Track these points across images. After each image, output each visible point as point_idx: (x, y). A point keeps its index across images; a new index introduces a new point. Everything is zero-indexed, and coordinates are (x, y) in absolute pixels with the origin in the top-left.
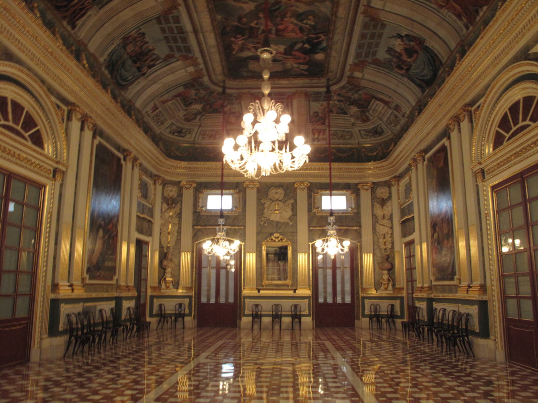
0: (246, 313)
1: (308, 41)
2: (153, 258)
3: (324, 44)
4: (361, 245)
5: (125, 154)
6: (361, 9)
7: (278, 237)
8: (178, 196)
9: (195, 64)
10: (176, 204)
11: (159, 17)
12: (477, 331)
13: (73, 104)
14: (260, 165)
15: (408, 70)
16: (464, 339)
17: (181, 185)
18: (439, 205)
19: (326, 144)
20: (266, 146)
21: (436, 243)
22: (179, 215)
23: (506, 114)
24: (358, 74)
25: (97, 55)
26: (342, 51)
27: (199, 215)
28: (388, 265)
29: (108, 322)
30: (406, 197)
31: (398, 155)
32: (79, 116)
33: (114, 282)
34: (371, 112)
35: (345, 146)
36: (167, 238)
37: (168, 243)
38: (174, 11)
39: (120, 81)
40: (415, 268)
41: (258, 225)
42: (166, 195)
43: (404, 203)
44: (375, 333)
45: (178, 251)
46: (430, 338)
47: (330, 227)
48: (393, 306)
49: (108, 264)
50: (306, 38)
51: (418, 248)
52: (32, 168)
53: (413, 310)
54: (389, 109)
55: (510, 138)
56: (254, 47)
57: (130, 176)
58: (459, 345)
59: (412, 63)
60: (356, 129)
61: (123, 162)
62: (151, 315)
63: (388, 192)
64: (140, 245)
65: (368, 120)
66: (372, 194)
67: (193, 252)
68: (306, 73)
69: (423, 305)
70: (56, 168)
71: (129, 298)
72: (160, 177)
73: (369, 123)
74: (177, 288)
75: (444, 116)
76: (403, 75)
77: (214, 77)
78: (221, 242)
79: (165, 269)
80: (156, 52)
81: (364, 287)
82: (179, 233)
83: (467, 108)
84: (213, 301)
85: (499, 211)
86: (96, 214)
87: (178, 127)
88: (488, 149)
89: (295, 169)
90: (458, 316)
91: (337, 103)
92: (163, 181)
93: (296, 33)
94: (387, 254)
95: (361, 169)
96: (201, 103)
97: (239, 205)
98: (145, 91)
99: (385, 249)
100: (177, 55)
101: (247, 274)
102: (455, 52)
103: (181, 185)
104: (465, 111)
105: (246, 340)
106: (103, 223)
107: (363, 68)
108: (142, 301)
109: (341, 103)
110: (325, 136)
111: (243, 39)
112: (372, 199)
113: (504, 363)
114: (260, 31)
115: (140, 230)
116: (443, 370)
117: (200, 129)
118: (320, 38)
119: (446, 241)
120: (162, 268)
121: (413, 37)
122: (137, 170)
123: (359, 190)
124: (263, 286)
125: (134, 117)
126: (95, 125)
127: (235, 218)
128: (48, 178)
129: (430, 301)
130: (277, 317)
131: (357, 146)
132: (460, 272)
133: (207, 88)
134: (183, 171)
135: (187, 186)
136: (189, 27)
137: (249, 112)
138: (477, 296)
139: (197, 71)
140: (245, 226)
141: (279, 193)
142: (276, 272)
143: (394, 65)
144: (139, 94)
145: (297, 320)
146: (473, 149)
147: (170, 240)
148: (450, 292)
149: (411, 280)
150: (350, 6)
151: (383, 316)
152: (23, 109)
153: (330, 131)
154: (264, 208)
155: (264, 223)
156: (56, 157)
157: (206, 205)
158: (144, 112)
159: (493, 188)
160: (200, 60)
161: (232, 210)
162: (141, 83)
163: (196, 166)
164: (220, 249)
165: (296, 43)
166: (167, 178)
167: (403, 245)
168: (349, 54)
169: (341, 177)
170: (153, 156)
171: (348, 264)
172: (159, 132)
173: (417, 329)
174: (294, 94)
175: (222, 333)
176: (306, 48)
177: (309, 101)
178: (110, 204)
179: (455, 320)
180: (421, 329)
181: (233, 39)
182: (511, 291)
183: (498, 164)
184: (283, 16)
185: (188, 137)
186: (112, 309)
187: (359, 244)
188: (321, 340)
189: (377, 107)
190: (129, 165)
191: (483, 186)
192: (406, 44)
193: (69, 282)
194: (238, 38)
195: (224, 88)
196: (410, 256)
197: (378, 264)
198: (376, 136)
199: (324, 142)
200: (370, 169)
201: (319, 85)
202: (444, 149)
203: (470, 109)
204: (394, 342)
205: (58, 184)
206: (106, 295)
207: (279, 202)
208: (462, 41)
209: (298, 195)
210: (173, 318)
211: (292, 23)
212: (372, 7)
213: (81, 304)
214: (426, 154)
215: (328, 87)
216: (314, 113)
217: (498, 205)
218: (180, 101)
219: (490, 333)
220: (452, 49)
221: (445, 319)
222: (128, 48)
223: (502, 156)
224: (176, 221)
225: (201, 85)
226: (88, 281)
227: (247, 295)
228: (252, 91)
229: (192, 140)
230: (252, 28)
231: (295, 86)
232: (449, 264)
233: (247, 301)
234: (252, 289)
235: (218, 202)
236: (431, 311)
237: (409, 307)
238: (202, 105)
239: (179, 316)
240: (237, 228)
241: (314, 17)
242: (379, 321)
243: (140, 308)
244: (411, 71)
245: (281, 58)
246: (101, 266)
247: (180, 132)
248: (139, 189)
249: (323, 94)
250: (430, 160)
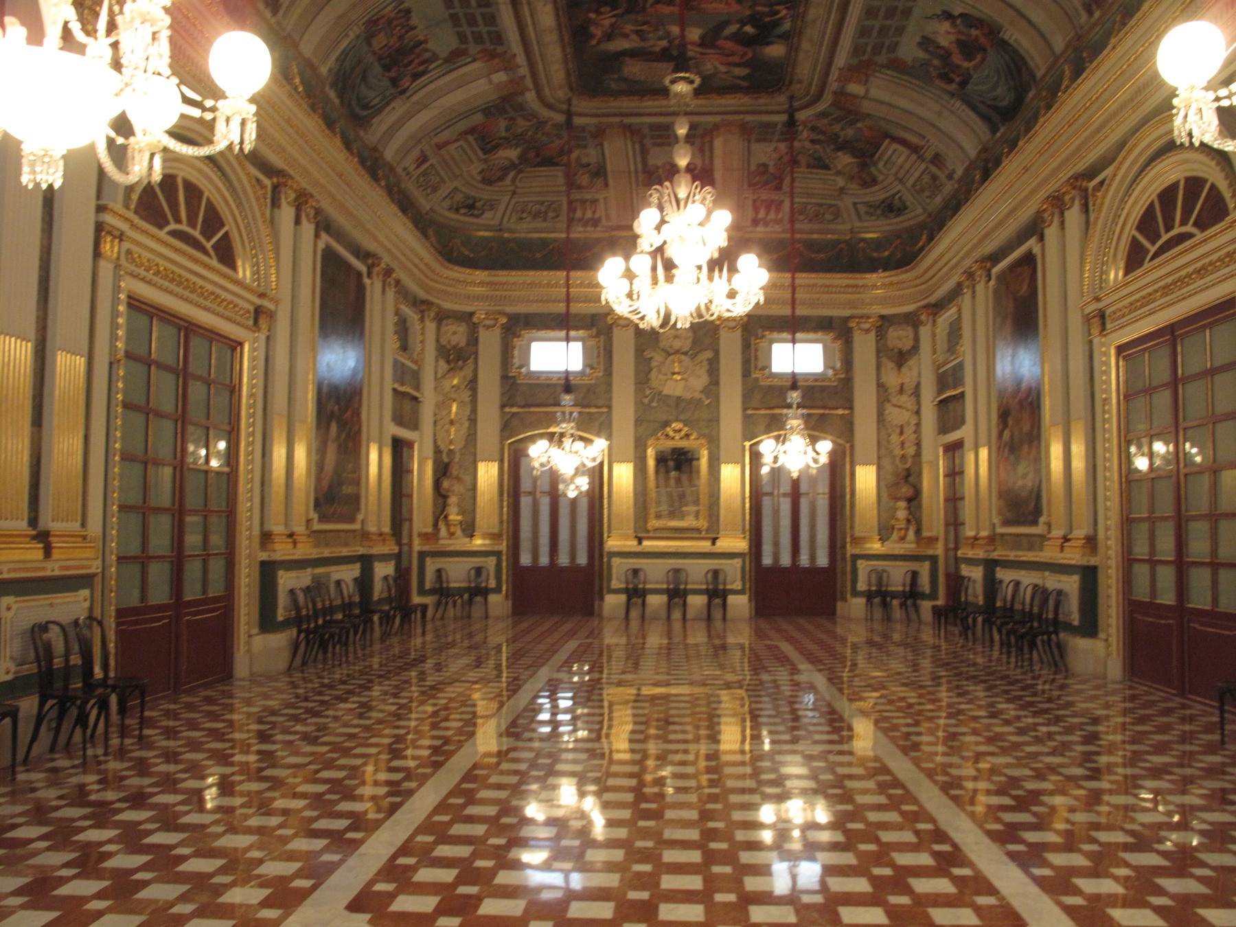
0: (613, 587)
1: (753, 20)
2: (422, 472)
3: (787, 25)
4: (852, 447)
5: (370, 261)
7: (680, 430)
8: (468, 344)
9: (508, 64)
10: (465, 361)
12: (1076, 623)
13: (280, 173)
14: (670, 307)
15: (963, 84)
16: (1050, 639)
17: (475, 320)
18: (1019, 364)
19: (783, 232)
20: (684, 273)
21: (1006, 450)
22: (473, 384)
23: (1152, 205)
24: (855, 88)
25: (315, 61)
26: (822, 44)
27: (514, 384)
28: (906, 490)
29: (351, 605)
30: (949, 350)
31: (936, 261)
32: (292, 196)
33: (357, 526)
34: (881, 165)
35: (823, 236)
36: (448, 431)
37: (451, 442)
39: (357, 110)
40: (962, 498)
41: (639, 404)
42: (443, 341)
43: (945, 364)
44: (878, 626)
45: (471, 459)
46: (987, 636)
47: (790, 412)
48: (915, 575)
49: (347, 490)
50: (748, 13)
51: (970, 457)
52: (220, 309)
53: (956, 583)
54: (918, 162)
56: (637, 32)
57: (380, 305)
58: (1040, 648)
59: (972, 72)
60: (848, 201)
61: (367, 281)
62: (422, 592)
63: (911, 336)
64: (399, 448)
65: (874, 181)
66: (877, 341)
67: (501, 461)
68: (745, 84)
69: (975, 574)
70: (259, 307)
71: (383, 558)
72: (432, 304)
73: (877, 188)
74: (472, 536)
75: (1034, 192)
76: (952, 95)
77: (547, 91)
78: (567, 442)
79: (445, 497)
80: (430, 45)
81: (857, 534)
82: (473, 420)
83: (1079, 183)
84: (544, 560)
85: (1128, 396)
86: (325, 390)
87: (468, 197)
88: (1115, 274)
89: (733, 315)
90: (1041, 593)
91: (808, 145)
92: (437, 314)
94: (907, 466)
95: (856, 286)
96: (517, 146)
97: (599, 363)
98: (403, 126)
99: (903, 456)
100: (474, 49)
101: (614, 508)
102: (1061, 61)
103: (475, 320)
104: (1074, 188)
105: (612, 637)
106: (336, 408)
107: (867, 76)
108: (405, 564)
109: (818, 147)
110: (780, 216)
112: (878, 351)
113: (1121, 683)
115: (399, 420)
116: (1007, 692)
117: (514, 200)
118: (778, 12)
119: (1025, 448)
120: (441, 495)
121: (977, 19)
122: (390, 293)
123: (850, 330)
124: (648, 531)
125: (383, 183)
126: (318, 211)
127: (590, 389)
128: (247, 327)
129: (990, 566)
130: (677, 594)
131: (848, 237)
132: (1049, 510)
134: (479, 290)
135: (488, 322)
137: (649, 205)
138: (1078, 557)
139: (511, 81)
140: (610, 407)
142: (664, 498)
143: (934, 74)
144: (391, 132)
145: (717, 601)
146: (1083, 267)
147: (456, 435)
148: (1031, 548)
149: (954, 522)
151: (894, 595)
152: (201, 193)
153: (792, 203)
154: (651, 370)
155: (652, 401)
156: (259, 285)
157: (526, 362)
158: (399, 170)
159: (1120, 349)
160: (521, 59)
161: (582, 373)
162: (399, 108)
163: (504, 279)
164: (565, 458)
166: (447, 305)
167: (941, 450)
168: (839, 48)
169: (812, 305)
170: (416, 261)
171: (823, 488)
172: (428, 208)
173: (962, 620)
174: (716, 127)
175: (567, 626)
176: (746, 33)
177: (749, 141)
179: (1036, 602)
180: (970, 620)
181: (592, 16)
182: (1141, 550)
183: (1131, 304)
185: (488, 218)
186: (355, 580)
187: (848, 445)
189: (894, 156)
190: (378, 285)
191: (1103, 345)
193: (286, 525)
194: (601, 13)
195: (569, 115)
196: (955, 473)
197: (887, 486)
198: (892, 215)
199: (777, 228)
200: (874, 287)
201: (772, 109)
202: (1029, 260)
203: (1084, 184)
204: (914, 645)
205: (263, 337)
206: (345, 552)
207: (683, 357)
208: (1079, 38)
209: (722, 341)
210: (466, 596)
213: (309, 570)
214: (994, 266)
215: (791, 116)
216: (759, 166)
217: (1126, 381)
218: (473, 143)
219: (1100, 628)
220: (1058, 50)
221: (1017, 599)
222: (374, 41)
223: (1140, 290)
224: (466, 395)
225: (520, 108)
226: (317, 526)
227: (616, 550)
228: (627, 120)
229: (496, 222)
231: (723, 109)
232: (1031, 492)
233: (616, 561)
234: (626, 537)
236: (991, 585)
237: (948, 576)
238: (519, 150)
239: (478, 592)
240: (593, 410)
242: (885, 605)
244: (969, 87)
246: (335, 495)
247: (471, 207)
248: (396, 333)
249: (779, 126)
250: (1002, 277)
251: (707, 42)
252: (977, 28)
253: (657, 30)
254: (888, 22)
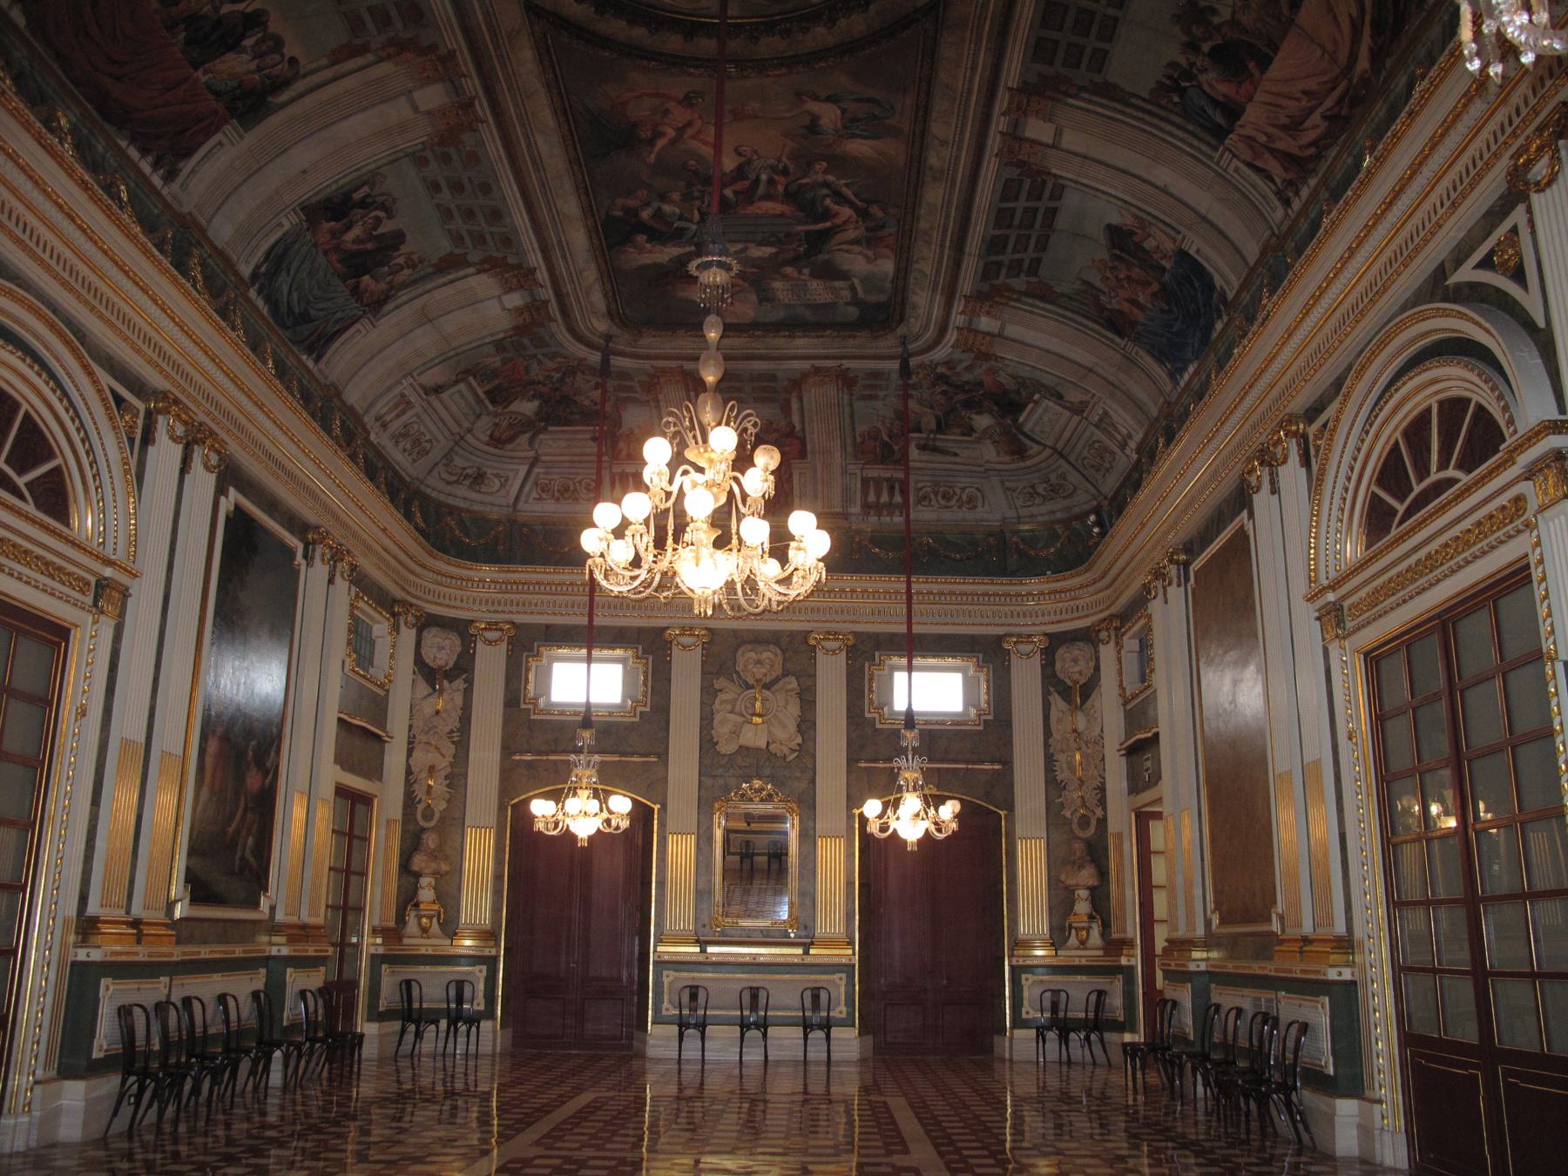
29: (242, 1033)
53: (1158, 1004)
55: (1409, 513)
57: (322, 597)
62: (375, 1015)
69: (1184, 996)
88: (1352, 549)
98: (378, 358)
141: (756, 663)
152: (15, 406)
174: (805, 375)
178: (256, 679)
186: (255, 995)
188: (881, 1094)
190: (320, 570)
195: (607, 354)
220: (1252, 262)
235: (586, 683)
243: (338, 995)
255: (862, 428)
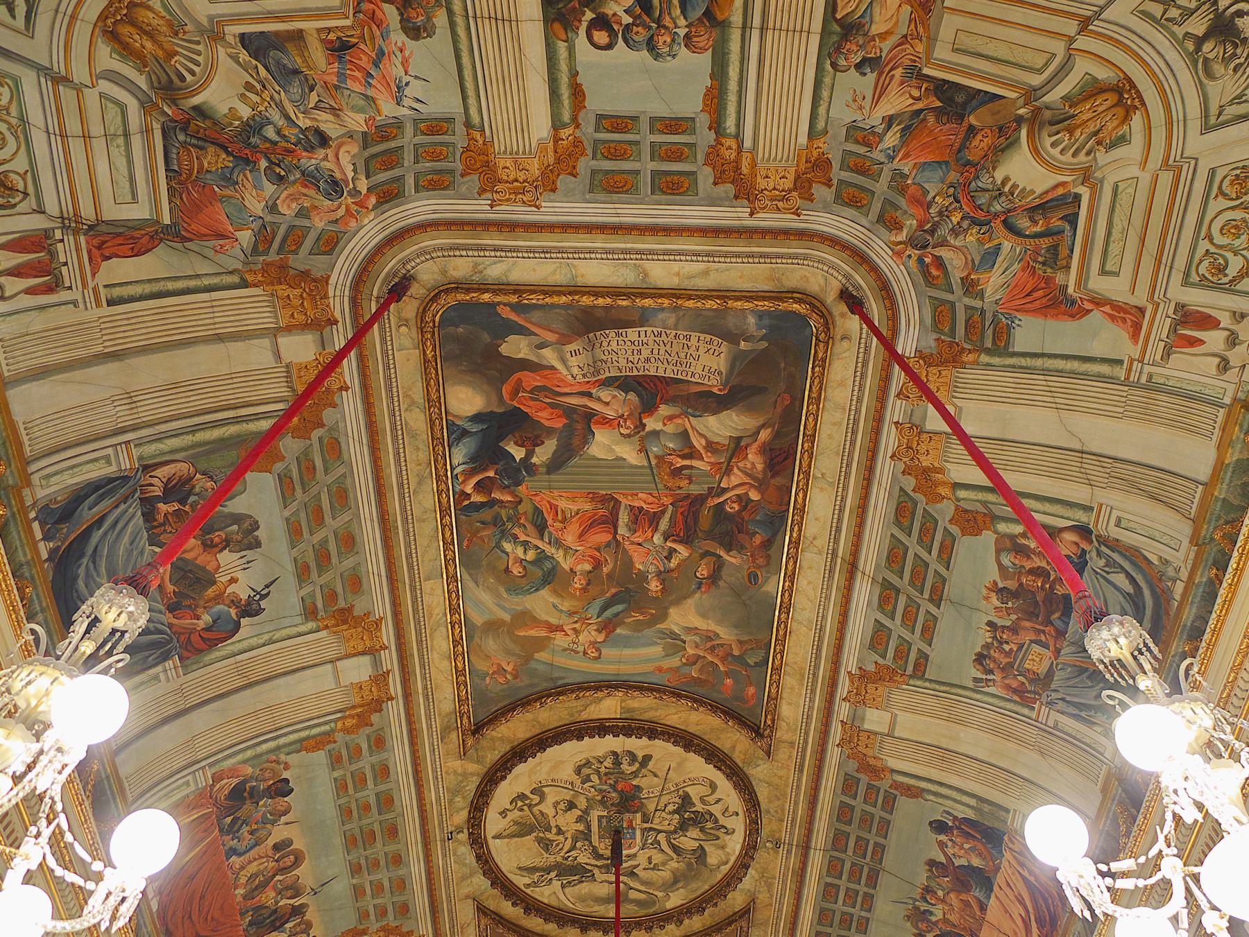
1: (515, 473)
3: (459, 455)
6: (387, 634)
9: (854, 731)
11: (911, 677)
15: (149, 504)
38: (871, 668)
56: (692, 454)
93: (554, 508)
100: (944, 511)
111: (724, 490)
114: (664, 524)
118: (479, 487)
133: (931, 273)
136: (863, 592)
150: (417, 622)
160: (890, 439)
165: (555, 465)
174: (547, 183)
177: (468, 124)
181: (754, 496)
184: (592, 577)
192: (219, 598)
211: (567, 549)
212: (363, 653)
225: (941, 315)
230: (686, 541)
241: (507, 570)
245: (605, 395)
251: (582, 423)
252: (208, 629)
253: (660, 458)
254: (316, 538)
255: (440, 42)
